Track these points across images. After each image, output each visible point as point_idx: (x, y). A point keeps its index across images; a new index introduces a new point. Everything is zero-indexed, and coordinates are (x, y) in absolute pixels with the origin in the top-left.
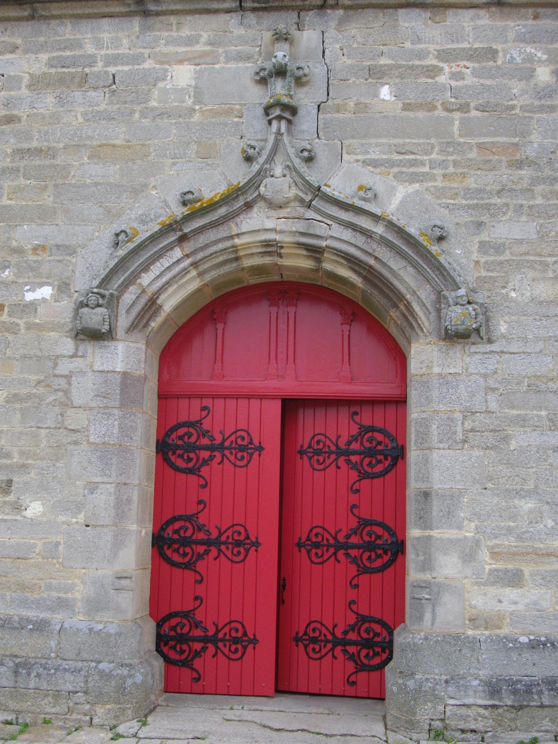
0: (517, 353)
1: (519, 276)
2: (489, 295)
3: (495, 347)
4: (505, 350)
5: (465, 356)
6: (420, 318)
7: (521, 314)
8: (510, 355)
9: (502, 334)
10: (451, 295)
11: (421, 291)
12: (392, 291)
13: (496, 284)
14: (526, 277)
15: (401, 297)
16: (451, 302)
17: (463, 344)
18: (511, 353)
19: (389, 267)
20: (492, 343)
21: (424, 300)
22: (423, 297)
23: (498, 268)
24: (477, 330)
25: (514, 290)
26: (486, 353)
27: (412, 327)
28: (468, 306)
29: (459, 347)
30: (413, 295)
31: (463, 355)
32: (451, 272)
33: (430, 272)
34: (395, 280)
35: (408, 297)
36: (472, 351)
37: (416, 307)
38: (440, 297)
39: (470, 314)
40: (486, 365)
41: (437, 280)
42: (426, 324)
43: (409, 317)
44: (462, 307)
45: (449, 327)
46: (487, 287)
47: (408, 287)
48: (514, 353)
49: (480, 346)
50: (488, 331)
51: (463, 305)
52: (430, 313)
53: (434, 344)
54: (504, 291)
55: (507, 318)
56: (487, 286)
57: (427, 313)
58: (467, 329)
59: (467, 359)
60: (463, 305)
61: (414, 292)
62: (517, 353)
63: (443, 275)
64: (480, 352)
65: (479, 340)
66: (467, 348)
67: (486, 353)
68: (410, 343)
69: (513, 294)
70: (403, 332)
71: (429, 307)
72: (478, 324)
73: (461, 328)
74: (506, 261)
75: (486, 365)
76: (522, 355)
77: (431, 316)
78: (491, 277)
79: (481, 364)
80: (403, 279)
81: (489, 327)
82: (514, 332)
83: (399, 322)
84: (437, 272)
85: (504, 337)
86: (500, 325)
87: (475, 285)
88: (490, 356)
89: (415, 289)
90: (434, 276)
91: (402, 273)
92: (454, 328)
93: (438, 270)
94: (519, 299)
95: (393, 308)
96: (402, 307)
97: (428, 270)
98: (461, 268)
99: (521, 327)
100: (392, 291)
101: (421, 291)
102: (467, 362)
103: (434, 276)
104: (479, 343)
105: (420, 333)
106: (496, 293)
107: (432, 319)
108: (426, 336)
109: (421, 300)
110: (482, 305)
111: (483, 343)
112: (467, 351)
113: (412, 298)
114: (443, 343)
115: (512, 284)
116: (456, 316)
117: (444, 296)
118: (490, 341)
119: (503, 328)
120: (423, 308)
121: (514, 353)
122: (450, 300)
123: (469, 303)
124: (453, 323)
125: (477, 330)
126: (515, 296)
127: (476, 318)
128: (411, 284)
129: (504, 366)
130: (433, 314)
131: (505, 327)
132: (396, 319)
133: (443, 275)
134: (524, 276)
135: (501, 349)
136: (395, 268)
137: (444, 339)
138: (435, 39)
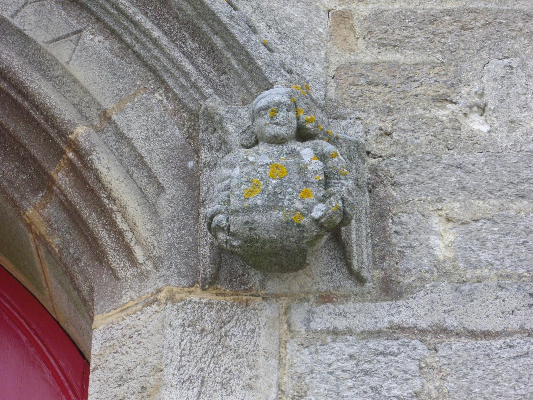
0: (497, 335)
1: (496, 66)
2: (388, 126)
3: (404, 313)
4: (451, 322)
5: (292, 346)
6: (123, 209)
7: (512, 191)
8: (471, 343)
9: (437, 265)
10: (235, 120)
11: (130, 114)
12: (29, 120)
13: (413, 88)
14: (523, 65)
15: (53, 135)
16: (234, 137)
17: (284, 302)
18: (473, 334)
19: (20, 33)
20: (399, 296)
21: (138, 144)
22: (136, 133)
23: (420, 37)
24: (335, 232)
25: (482, 109)
26: (378, 334)
27: (99, 255)
28: (297, 146)
29: (269, 311)
30: (100, 131)
31: (282, 344)
32: (235, 31)
33: (164, 41)
34: (36, 75)
35: (80, 131)
36: (317, 325)
37: (109, 170)
38: (199, 128)
39: (302, 170)
40: (375, 381)
41: (187, 66)
42: (144, 226)
43: (86, 212)
44: (274, 149)
45: (220, 218)
46: (380, 99)
47: (84, 104)
48: (486, 335)
49: (351, 306)
50: (382, 251)
51: (277, 140)
52: (161, 189)
53: (171, 298)
54: (443, 113)
55: (454, 207)
56: (379, 95)
57: (151, 190)
58: (288, 224)
59: (301, 359)
60: (277, 140)
61: (105, 116)
62: (497, 335)
63: (211, 52)
64: (349, 331)
65: (348, 285)
66: (298, 316)
67: (378, 334)
68: (86, 307)
69: (477, 124)
70: (72, 279)
71: (157, 168)
72: (335, 203)
73: (268, 222)
74: (449, 12)
75: (375, 381)
76: (517, 339)
77: (162, 202)
78: (394, 66)
79: (353, 375)
80: (66, 73)
81: (386, 239)
82: (484, 256)
83: (55, 241)
84: (192, 45)
85: (446, 274)
86: (429, 231)
87: (332, 92)
88: (393, 346)
89: (108, 105)
90: (177, 54)
91: (62, 52)
92: (237, 221)
93: (195, 32)
94: (502, 139)
95: (35, 192)
96: (62, 178)
97: (156, 33)
98: (283, 36)
99: (510, 240)
100: (29, 120)
101: (130, 114)
102: (301, 369)
103: (177, 54)
104: (346, 298)
105: (125, 272)
106: (413, 119)
107: (165, 207)
108: (144, 275)
109: (129, 142)
110: (358, 151)
111: (362, 297)
112: (299, 326)
113: (95, 137)
114: (207, 297)
115: (476, 86)
116: (248, 181)
117: (209, 116)
118: (390, 290)
119: (443, 242)
120: (137, 173)
121: (486, 335)
122: (230, 127)
123: (303, 135)
124: (235, 204)
125: (335, 232)
126: (485, 128)
127: (327, 185)
128: (94, 90)
129: (450, 384)
130: (173, 190)
131: (450, 237)
132: (43, 230)
133: (211, 52)
134: (515, 62)
135: (436, 318)
136: (40, 37)
137: (210, 283)
138: (453, 88)
